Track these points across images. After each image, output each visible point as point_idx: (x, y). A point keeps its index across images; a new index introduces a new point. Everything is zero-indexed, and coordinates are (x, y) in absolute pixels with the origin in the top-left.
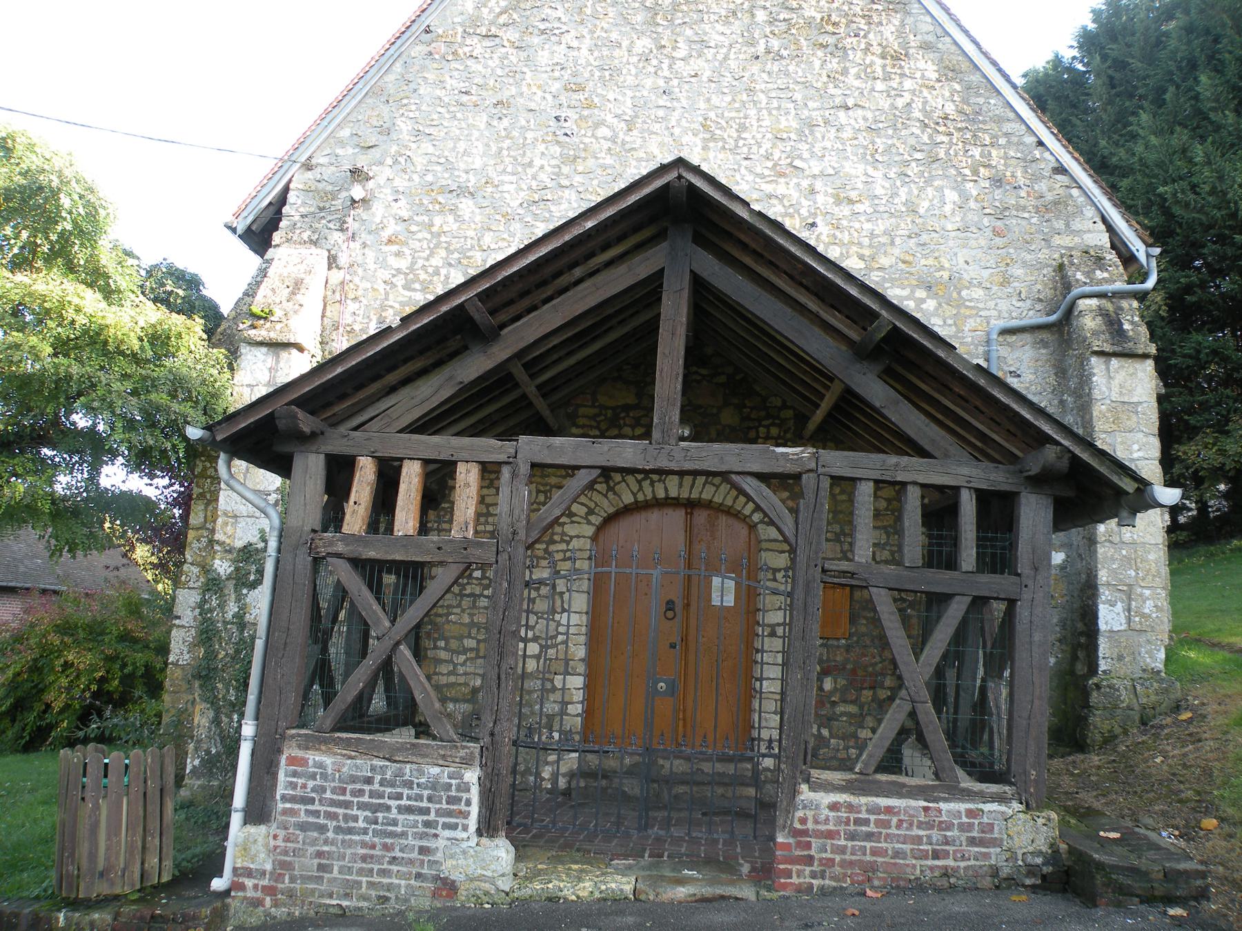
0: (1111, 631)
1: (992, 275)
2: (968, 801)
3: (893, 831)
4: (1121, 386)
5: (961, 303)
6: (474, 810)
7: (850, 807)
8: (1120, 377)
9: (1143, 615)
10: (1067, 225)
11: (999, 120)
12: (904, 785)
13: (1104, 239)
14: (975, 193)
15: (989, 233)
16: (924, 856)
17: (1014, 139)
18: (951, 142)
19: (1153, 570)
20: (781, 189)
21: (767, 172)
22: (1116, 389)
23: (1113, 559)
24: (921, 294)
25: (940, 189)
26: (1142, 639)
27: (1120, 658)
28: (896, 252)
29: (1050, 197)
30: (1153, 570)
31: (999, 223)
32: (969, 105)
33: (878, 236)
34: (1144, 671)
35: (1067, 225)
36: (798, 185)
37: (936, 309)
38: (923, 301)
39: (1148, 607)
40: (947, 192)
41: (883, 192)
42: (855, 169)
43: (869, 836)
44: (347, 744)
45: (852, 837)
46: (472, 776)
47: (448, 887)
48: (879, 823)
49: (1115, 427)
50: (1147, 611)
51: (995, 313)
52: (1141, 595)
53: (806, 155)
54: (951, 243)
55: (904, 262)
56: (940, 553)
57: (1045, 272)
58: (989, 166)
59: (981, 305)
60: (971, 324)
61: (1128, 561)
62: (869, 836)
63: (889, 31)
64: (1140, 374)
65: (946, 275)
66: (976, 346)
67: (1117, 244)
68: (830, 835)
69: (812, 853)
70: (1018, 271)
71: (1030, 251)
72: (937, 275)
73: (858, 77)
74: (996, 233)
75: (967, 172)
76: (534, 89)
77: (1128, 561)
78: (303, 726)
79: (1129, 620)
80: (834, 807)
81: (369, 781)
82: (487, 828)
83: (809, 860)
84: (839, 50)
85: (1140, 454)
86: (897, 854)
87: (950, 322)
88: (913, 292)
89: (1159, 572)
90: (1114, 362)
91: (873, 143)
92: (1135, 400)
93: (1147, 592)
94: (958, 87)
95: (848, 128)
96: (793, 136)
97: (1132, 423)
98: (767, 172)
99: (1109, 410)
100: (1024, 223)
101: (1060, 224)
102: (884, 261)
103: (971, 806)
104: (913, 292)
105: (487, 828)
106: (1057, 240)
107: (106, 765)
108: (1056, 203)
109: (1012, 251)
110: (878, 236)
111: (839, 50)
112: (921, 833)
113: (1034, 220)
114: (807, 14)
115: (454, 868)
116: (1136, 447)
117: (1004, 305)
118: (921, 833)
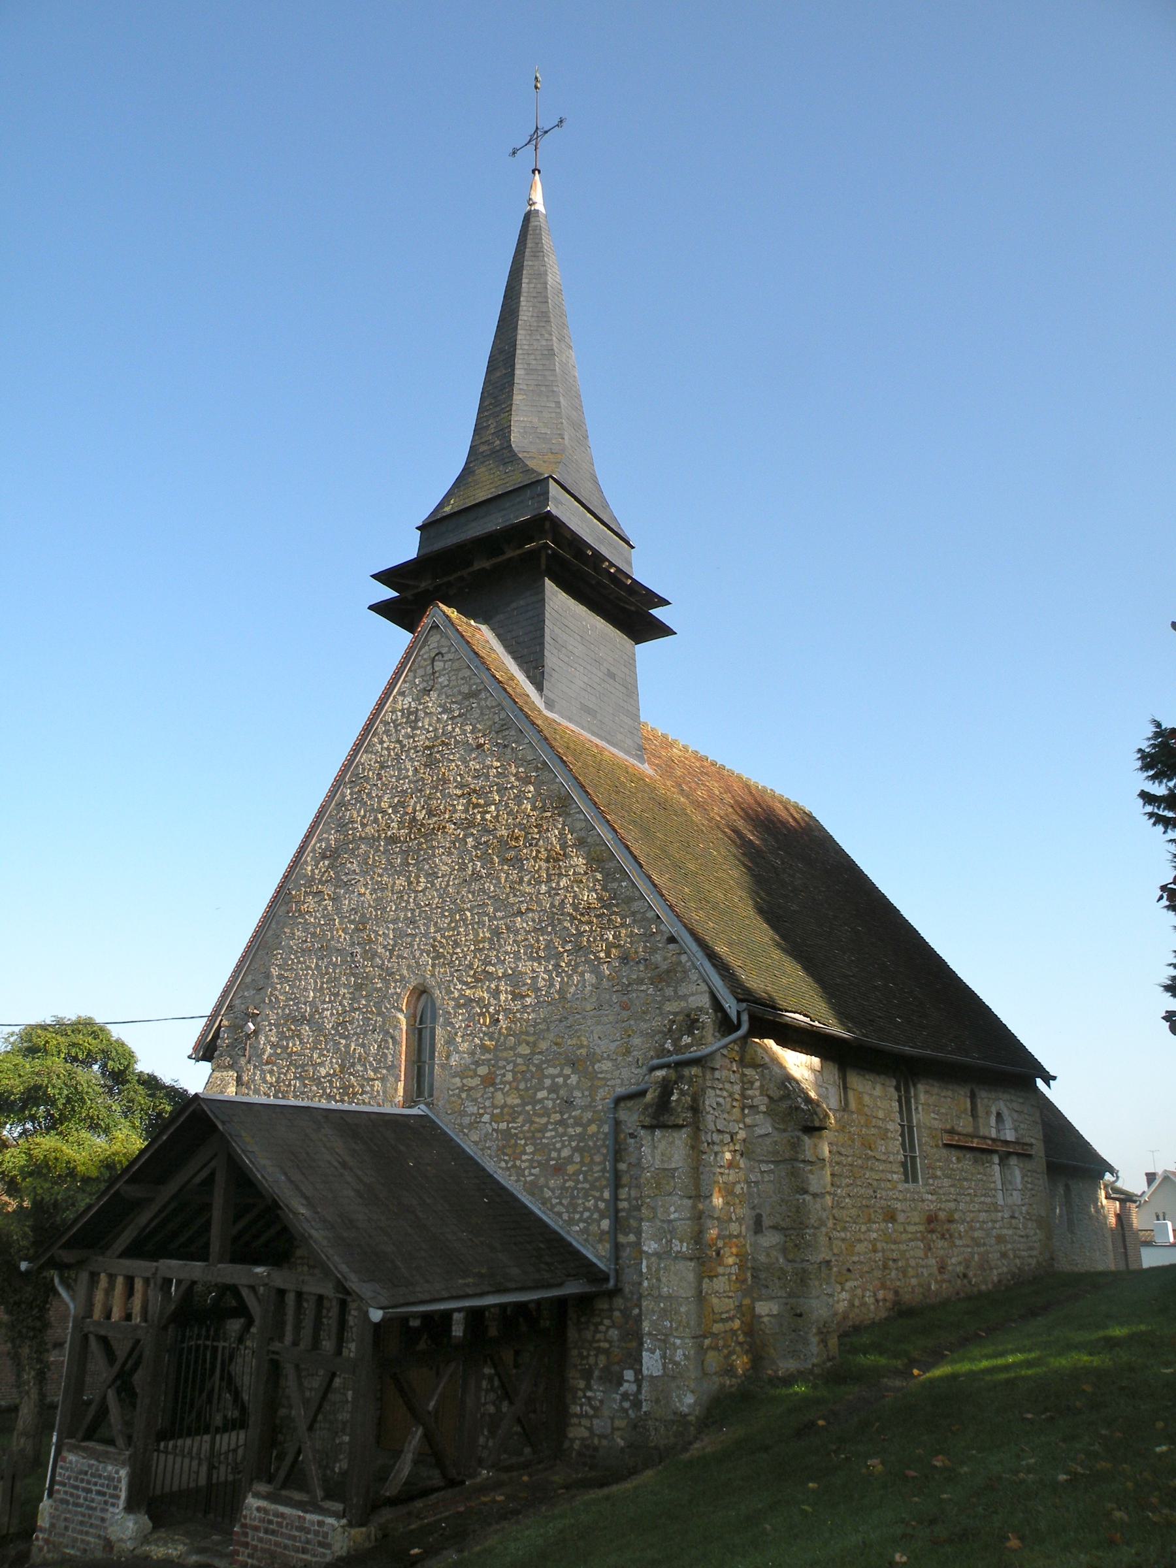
0: (651, 1376)
1: (617, 1047)
2: (320, 1514)
3: (284, 1530)
4: (663, 1155)
5: (593, 1076)
6: (123, 1495)
7: (266, 1511)
8: (662, 1146)
9: (677, 1364)
10: (676, 992)
11: (629, 900)
12: (291, 1499)
13: (705, 1001)
14: (607, 972)
15: (617, 1008)
16: (297, 1550)
17: (639, 916)
18: (591, 931)
19: (684, 1321)
20: (479, 993)
21: (469, 980)
22: (658, 1157)
23: (653, 1312)
24: (567, 1071)
25: (582, 974)
26: (673, 1385)
27: (657, 1401)
28: (551, 1036)
29: (664, 966)
30: (684, 1321)
31: (625, 998)
32: (607, 891)
33: (540, 1023)
34: (675, 1413)
35: (676, 992)
36: (489, 987)
37: (578, 1083)
38: (568, 1077)
39: (679, 1355)
40: (587, 976)
41: (543, 983)
42: (525, 966)
43: (273, 1532)
44: (85, 1449)
45: (266, 1531)
46: (123, 1473)
47: (109, 1545)
48: (280, 1524)
49: (657, 1192)
50: (677, 1359)
51: (619, 1081)
52: (674, 1344)
53: (494, 961)
54: (589, 1022)
55: (556, 1044)
56: (215, 1349)
57: (657, 1038)
58: (619, 946)
59: (609, 1076)
60: (601, 1093)
61: (664, 1313)
62: (273, 1532)
63: (553, 835)
64: (677, 1142)
65: (583, 1051)
66: (605, 1113)
67: (717, 1005)
68: (256, 1529)
69: (249, 1540)
70: (637, 1041)
71: (645, 1021)
72: (578, 1052)
73: (529, 883)
74: (625, 1007)
75: (602, 955)
76: (340, 932)
77: (664, 1313)
78: (72, 1438)
79: (664, 1365)
80: (259, 1509)
81: (86, 1473)
82: (130, 1508)
83: (246, 1545)
84: (517, 862)
85: (676, 1215)
86: (286, 1547)
87: (587, 1093)
88: (562, 1070)
89: (688, 1323)
90: (657, 1133)
91: (538, 941)
92: (673, 1166)
93: (678, 1342)
94: (599, 876)
95: (522, 931)
96: (487, 945)
97: (669, 1188)
98: (469, 980)
99: (652, 1177)
100: (642, 995)
101: (669, 992)
102: (543, 1045)
103: (320, 1518)
104: (562, 1070)
105: (130, 1508)
106: (668, 1007)
107: (813, 1424)
108: (668, 971)
109: (632, 1022)
110: (540, 1023)
111: (517, 862)
112: (297, 1534)
113: (650, 991)
114: (499, 834)
115: (114, 1533)
116: (672, 1209)
117: (625, 1073)
118: (297, 1534)
